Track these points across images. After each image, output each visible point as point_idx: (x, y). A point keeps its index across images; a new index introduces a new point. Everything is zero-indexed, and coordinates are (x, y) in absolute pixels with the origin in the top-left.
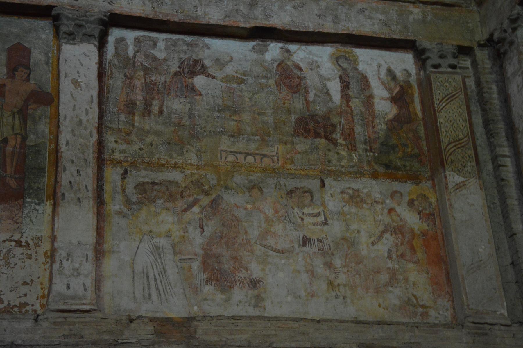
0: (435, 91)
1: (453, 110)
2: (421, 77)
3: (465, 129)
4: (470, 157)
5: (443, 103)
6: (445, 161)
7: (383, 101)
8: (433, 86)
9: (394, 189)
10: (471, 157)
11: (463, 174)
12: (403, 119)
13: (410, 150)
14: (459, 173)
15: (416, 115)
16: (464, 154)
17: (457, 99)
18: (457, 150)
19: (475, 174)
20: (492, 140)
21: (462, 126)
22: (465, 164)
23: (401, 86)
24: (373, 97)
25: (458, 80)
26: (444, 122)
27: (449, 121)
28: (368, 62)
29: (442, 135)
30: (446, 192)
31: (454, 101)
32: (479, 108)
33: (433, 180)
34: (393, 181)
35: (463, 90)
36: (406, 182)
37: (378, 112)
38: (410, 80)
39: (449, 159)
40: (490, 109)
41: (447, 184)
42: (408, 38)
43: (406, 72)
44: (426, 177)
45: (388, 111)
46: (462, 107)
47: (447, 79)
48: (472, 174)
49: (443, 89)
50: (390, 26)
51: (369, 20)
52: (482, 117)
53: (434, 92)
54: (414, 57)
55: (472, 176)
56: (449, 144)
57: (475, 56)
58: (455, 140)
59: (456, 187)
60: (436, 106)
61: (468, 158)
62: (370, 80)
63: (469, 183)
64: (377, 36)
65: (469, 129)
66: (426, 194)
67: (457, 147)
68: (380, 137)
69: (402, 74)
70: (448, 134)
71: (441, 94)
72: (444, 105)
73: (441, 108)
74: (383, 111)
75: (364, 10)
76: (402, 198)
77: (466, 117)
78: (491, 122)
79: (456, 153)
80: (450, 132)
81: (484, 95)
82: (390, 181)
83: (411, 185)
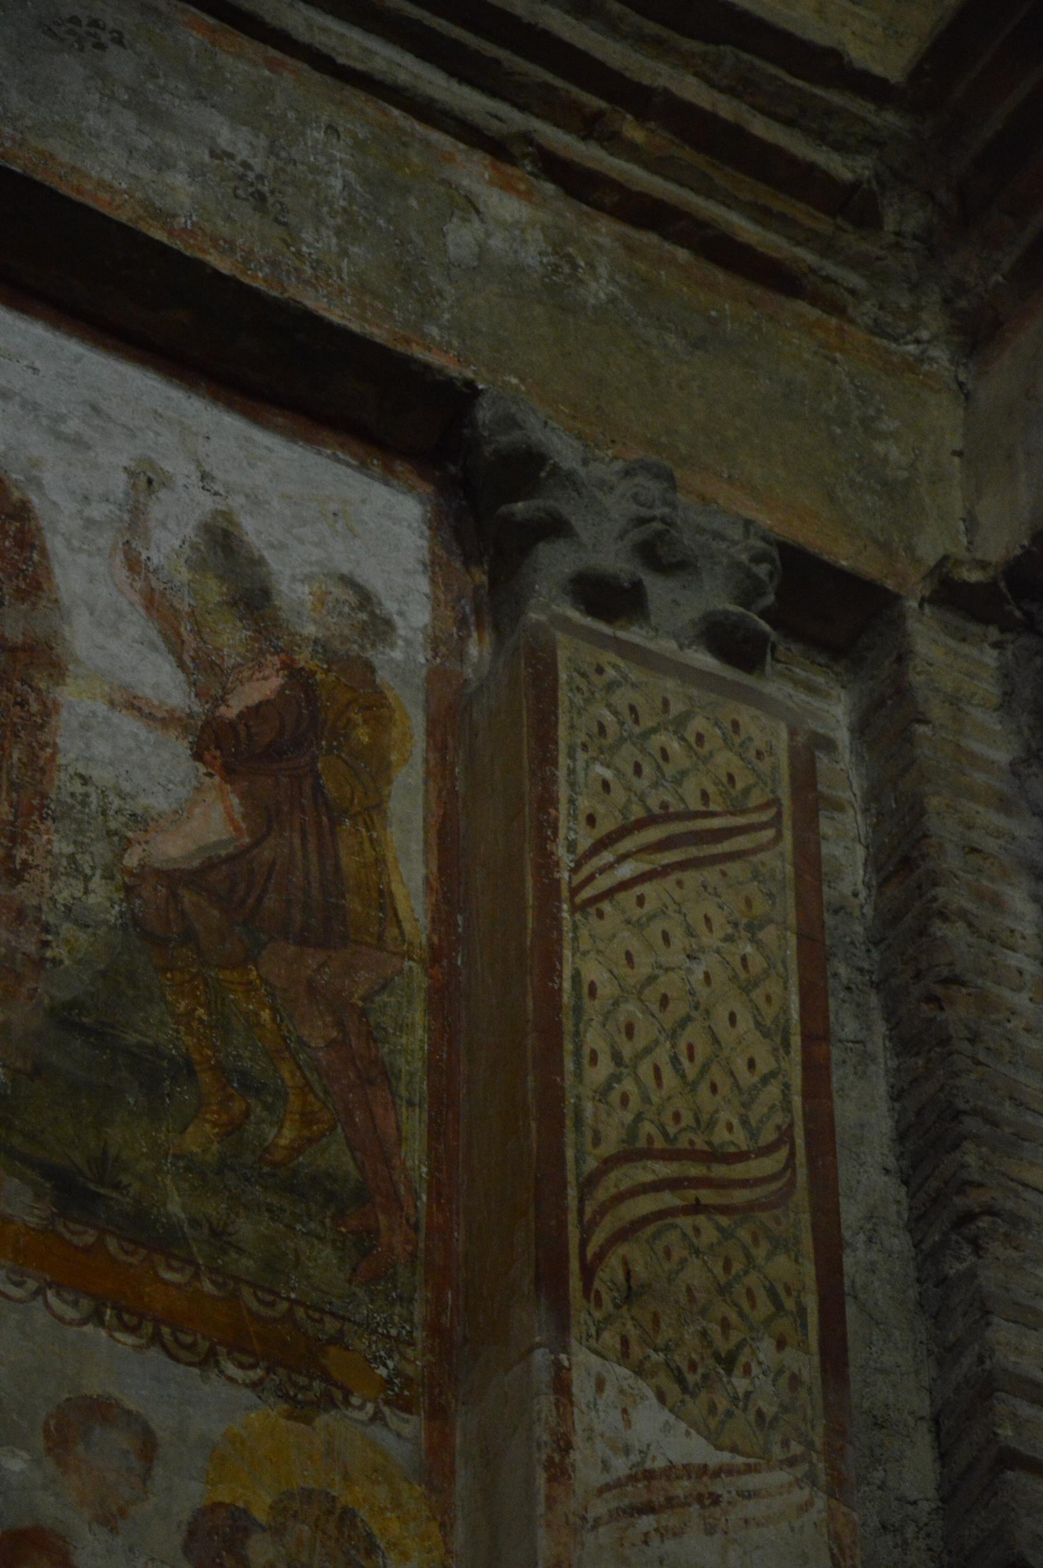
0: (571, 756)
1: (690, 932)
2: (469, 672)
3: (774, 1090)
4: (779, 1306)
5: (622, 858)
6: (574, 1265)
7: (129, 724)
8: (563, 720)
9: (95, 1385)
10: (789, 1304)
11: (712, 1409)
12: (271, 901)
13: (288, 1135)
14: (673, 1390)
15: (381, 908)
16: (737, 1267)
17: (734, 869)
18: (685, 1222)
19: (810, 1445)
20: (953, 1268)
21: (751, 1064)
22: (735, 1337)
23: (295, 674)
24: (57, 670)
25: (759, 743)
26: (607, 990)
27: (652, 995)
28: (61, 418)
29: (579, 1075)
30: (551, 1501)
31: (711, 875)
32: (881, 1028)
33: (438, 1414)
34: (96, 1317)
35: (787, 821)
36: (208, 1361)
37: (78, 788)
38: (377, 657)
39: (613, 1261)
40: (974, 1039)
41: (565, 1445)
42: (418, 352)
43: (354, 600)
44: (389, 1382)
45: (159, 803)
46: (769, 934)
47: (677, 708)
48: (776, 1437)
49: (638, 770)
50: (292, 219)
51: (129, 120)
52: (896, 1096)
53: (563, 760)
54: (435, 524)
55: (777, 1452)
56: (630, 1155)
57: (902, 658)
58: (683, 1143)
59: (637, 1493)
60: (566, 859)
61: (764, 1307)
62: (56, 544)
63: (748, 1495)
64: (177, 245)
65: (797, 1101)
66: (363, 1513)
67: (691, 1194)
68: (56, 962)
69: (321, 600)
70: (628, 1085)
71: (619, 795)
72: (626, 871)
73: (603, 882)
74: (122, 795)
75: (105, 37)
76: (146, 1476)
77: (785, 1010)
78: (971, 1124)
79: (672, 1237)
80: (645, 1069)
81: (939, 929)
82: (70, 1313)
83: (248, 1396)
